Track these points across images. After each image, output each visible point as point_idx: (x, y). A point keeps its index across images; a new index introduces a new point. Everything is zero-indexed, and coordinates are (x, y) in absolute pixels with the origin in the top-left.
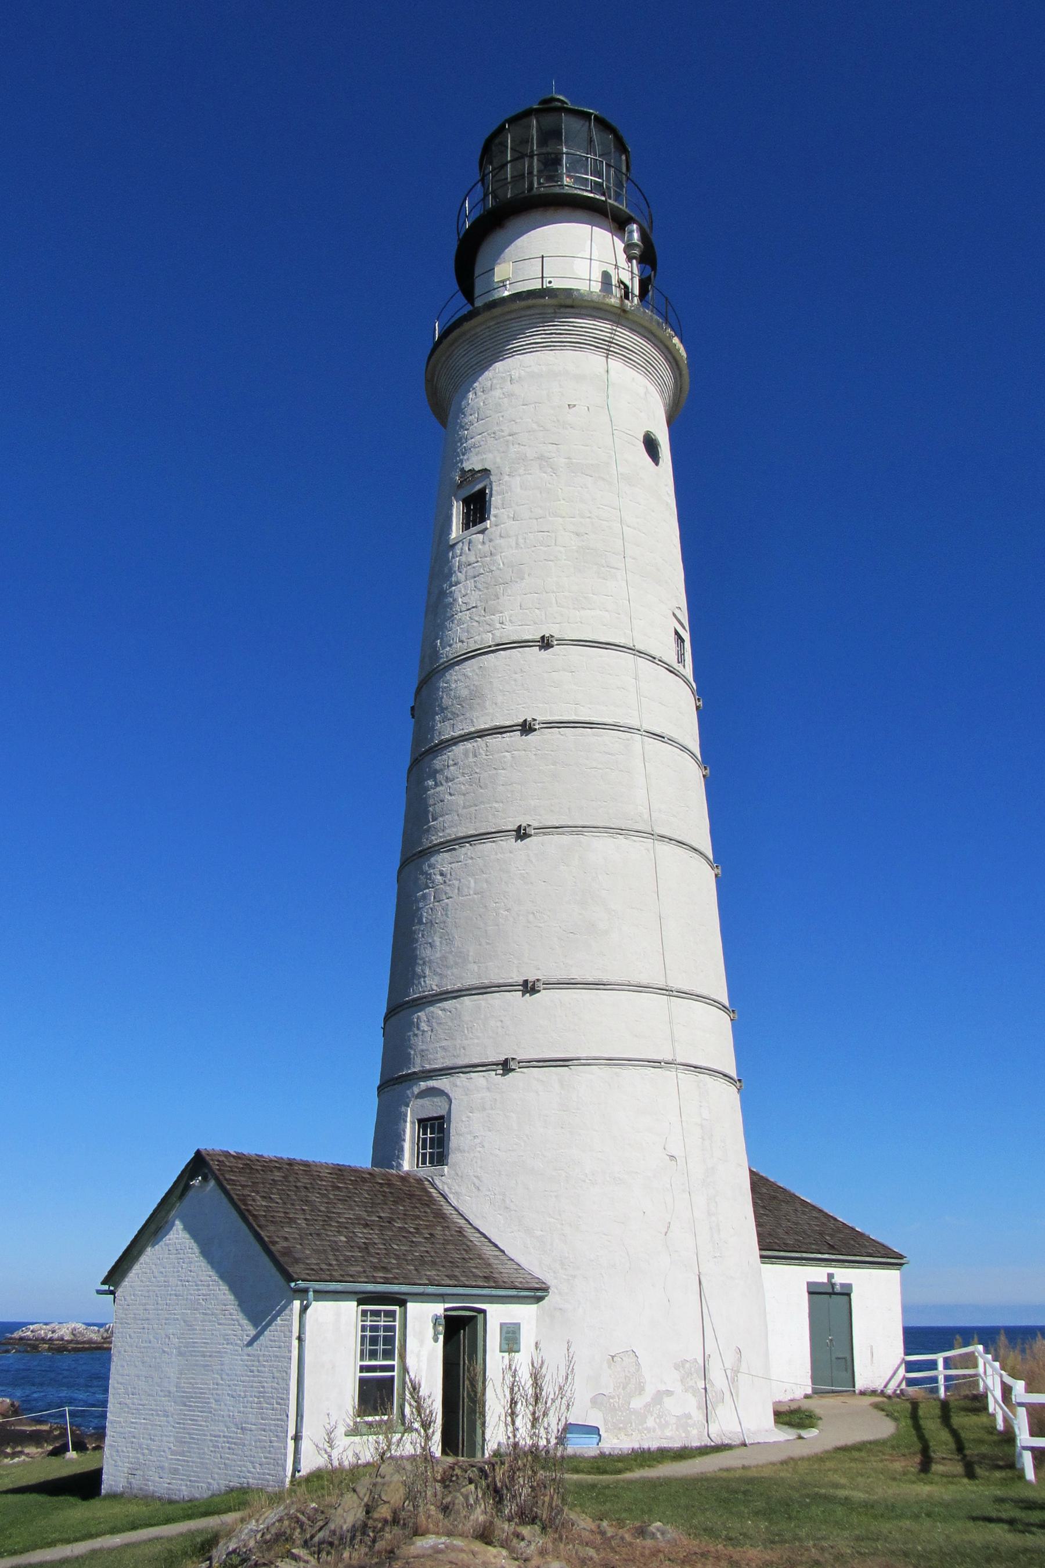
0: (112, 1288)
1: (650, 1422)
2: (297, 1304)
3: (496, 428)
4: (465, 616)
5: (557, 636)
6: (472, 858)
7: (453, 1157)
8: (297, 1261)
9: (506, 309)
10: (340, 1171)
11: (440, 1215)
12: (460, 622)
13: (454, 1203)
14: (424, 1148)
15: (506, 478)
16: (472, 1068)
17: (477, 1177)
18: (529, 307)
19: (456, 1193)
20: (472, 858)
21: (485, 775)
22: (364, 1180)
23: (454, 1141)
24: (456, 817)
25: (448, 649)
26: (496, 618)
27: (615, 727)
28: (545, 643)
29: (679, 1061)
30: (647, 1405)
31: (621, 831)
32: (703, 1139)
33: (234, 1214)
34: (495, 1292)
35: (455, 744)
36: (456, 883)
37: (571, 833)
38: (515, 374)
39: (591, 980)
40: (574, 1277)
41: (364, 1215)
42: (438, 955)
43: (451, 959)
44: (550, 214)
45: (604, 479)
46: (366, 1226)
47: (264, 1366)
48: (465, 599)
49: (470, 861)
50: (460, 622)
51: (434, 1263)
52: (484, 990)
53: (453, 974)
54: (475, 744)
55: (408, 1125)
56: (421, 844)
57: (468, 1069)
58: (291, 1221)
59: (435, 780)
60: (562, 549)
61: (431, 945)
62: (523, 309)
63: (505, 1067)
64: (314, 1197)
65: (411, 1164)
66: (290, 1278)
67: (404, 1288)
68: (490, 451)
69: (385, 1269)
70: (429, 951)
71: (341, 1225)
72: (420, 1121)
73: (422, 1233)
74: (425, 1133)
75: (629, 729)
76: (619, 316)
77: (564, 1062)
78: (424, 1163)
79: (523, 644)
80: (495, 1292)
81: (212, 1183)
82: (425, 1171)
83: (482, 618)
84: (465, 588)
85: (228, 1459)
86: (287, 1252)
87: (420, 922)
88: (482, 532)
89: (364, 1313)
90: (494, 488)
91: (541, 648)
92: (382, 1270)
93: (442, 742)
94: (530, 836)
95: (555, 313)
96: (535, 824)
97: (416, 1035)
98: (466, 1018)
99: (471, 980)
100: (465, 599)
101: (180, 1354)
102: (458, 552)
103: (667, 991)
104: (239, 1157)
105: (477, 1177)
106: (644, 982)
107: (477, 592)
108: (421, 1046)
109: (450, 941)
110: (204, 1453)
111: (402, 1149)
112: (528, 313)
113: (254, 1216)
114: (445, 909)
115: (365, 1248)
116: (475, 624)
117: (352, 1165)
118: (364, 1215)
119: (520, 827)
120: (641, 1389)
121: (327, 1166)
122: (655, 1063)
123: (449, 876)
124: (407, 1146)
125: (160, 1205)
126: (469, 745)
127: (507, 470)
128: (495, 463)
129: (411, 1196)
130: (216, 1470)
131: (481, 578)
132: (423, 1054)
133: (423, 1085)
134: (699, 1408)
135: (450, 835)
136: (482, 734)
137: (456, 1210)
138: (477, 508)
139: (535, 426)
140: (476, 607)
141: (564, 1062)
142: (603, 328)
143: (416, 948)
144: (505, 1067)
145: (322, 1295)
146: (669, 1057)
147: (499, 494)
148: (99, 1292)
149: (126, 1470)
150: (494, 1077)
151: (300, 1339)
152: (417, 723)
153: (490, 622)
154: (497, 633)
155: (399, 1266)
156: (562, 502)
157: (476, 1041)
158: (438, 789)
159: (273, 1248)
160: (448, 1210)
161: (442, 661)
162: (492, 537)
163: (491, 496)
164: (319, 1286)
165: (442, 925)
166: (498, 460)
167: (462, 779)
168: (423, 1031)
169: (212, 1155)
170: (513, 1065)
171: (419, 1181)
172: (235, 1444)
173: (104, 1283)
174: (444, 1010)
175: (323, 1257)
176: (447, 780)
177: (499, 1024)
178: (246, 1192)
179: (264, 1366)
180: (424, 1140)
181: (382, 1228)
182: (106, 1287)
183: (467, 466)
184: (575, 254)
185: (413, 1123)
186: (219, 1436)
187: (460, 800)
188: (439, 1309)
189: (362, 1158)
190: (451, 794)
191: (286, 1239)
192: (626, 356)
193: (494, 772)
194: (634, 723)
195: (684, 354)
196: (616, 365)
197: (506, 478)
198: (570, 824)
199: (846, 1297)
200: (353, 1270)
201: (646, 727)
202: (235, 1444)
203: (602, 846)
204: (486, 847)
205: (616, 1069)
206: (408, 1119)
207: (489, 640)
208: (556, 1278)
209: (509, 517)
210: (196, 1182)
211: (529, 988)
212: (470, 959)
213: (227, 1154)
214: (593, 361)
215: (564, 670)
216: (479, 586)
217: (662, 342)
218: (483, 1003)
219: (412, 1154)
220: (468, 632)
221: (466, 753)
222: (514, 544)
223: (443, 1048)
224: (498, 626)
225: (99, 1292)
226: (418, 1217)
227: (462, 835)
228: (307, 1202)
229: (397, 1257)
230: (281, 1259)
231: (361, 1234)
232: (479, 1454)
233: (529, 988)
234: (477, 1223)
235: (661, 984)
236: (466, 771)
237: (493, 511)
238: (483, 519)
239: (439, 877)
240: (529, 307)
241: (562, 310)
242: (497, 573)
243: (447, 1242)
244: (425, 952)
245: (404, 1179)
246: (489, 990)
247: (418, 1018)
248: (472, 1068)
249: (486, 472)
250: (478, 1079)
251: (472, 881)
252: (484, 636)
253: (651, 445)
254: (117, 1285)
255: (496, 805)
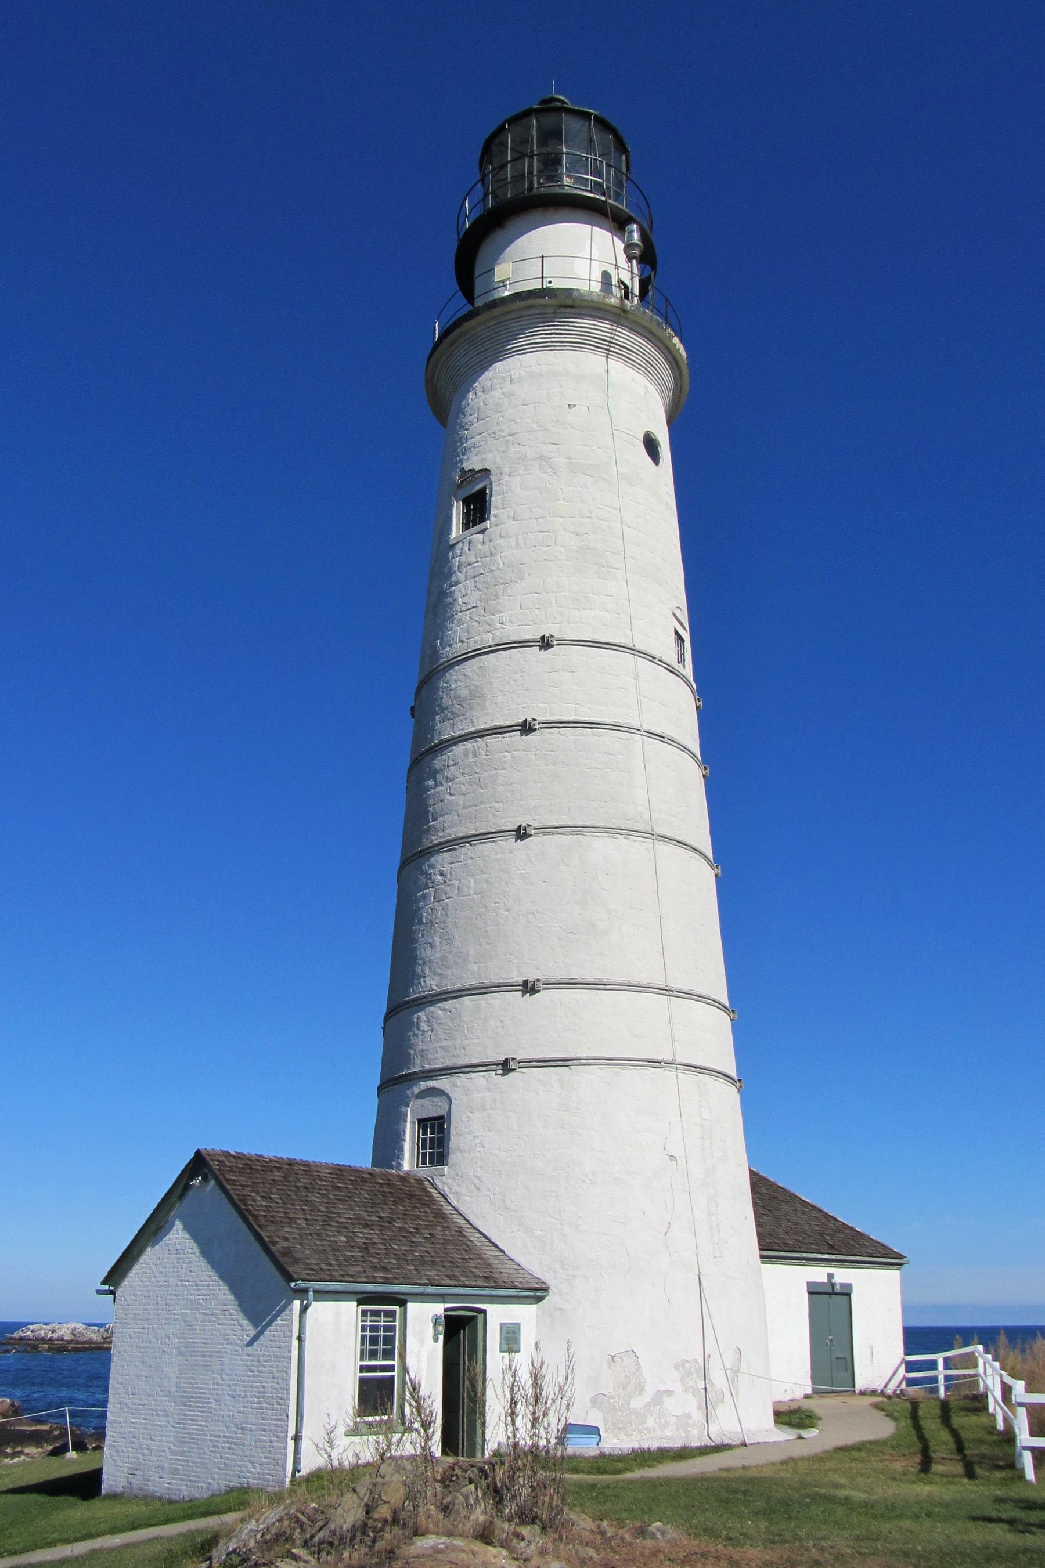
0: (112, 1288)
1: (650, 1422)
2: (297, 1304)
3: (496, 428)
4: (465, 616)
5: (557, 636)
6: (472, 858)
7: (453, 1157)
8: (297, 1261)
9: (506, 309)
10: (340, 1171)
11: (440, 1215)
12: (460, 622)
13: (454, 1203)
14: (424, 1148)
15: (506, 478)
16: (472, 1068)
17: (477, 1177)
18: (529, 307)
19: (456, 1193)
20: (472, 858)
21: (485, 775)
22: (364, 1180)
23: (454, 1141)
24: (456, 817)
25: (448, 649)
26: (496, 618)
27: (615, 727)
28: (545, 643)
29: (679, 1061)
30: (647, 1405)
31: (621, 831)
32: (703, 1139)
33: (234, 1214)
34: (495, 1292)
35: (455, 744)
36: (456, 883)
37: (571, 833)
38: (515, 374)
39: (591, 980)
40: (574, 1277)
41: (364, 1215)
42: (438, 955)
43: (451, 959)
44: (550, 214)
45: (604, 479)
46: (366, 1226)
47: (264, 1366)
48: (465, 599)
49: (470, 861)
50: (460, 622)
51: (434, 1263)
52: (484, 990)
53: (453, 974)
54: (475, 744)
55: (408, 1125)
56: (421, 844)
57: (468, 1069)
58: (291, 1221)
59: (435, 780)
60: (562, 549)
61: (431, 945)
62: (523, 309)
63: (505, 1067)
64: (314, 1197)
65: (411, 1164)
66: (290, 1278)
67: (404, 1288)
68: (490, 451)
69: (385, 1269)
70: (429, 951)
71: (341, 1225)
72: (420, 1121)
73: (422, 1233)
74: (425, 1133)
75: (629, 729)
76: (619, 316)
77: (564, 1062)
78: (424, 1163)
79: (523, 644)
80: (495, 1292)
81: (212, 1183)
82: (425, 1171)
83: (482, 618)
84: (465, 588)
85: (228, 1459)
86: (287, 1252)
87: (420, 922)
88: (482, 532)
89: (364, 1313)
90: (494, 488)
91: (541, 648)
92: (382, 1270)
93: (442, 742)
94: (530, 836)
95: (555, 313)
96: (535, 824)
97: (416, 1035)
98: (466, 1018)
99: (471, 980)
100: (465, 599)
101: (180, 1354)
102: (458, 552)
103: (667, 991)
104: (239, 1157)
105: (477, 1177)
106: (644, 982)
107: (477, 592)
108: (421, 1046)
109: (450, 941)
110: (204, 1453)
111: (402, 1149)
112: (528, 313)
113: (254, 1216)
114: (445, 909)
115: (365, 1248)
116: (475, 624)
117: (352, 1165)
118: (364, 1215)
119: (520, 827)
120: (641, 1389)
121: (327, 1166)
122: (655, 1063)
123: (449, 876)
124: (407, 1146)
125: (160, 1205)
126: (469, 745)
127: (507, 470)
128: (495, 463)
129: (411, 1196)
130: (216, 1470)
131: (481, 578)
132: (423, 1054)
133: (423, 1085)
134: (699, 1408)
135: (450, 835)
136: (482, 734)
137: (456, 1210)
138: (477, 508)
139: (535, 426)
140: (476, 607)
141: (564, 1062)
142: (603, 328)
143: (416, 948)
144: (505, 1067)
145: (322, 1295)
146: (669, 1057)
147: (499, 494)
148: (99, 1292)
149: (126, 1470)
150: (494, 1077)
151: (300, 1339)
152: (417, 723)
153: (490, 622)
154: (497, 633)
155: (399, 1266)
156: (562, 502)
157: (476, 1041)
158: (438, 789)
159: (273, 1248)
160: (448, 1210)
161: (442, 661)
162: (492, 537)
163: (491, 496)
164: (319, 1286)
165: (442, 925)
166: (498, 460)
167: (462, 779)
168: (423, 1031)
169: (212, 1155)
170: (513, 1065)
171: (419, 1181)
172: (235, 1444)
173: (104, 1283)
174: (444, 1010)
175: (323, 1257)
176: (447, 780)
177: (499, 1024)
178: (246, 1192)
179: (264, 1366)
180: (424, 1140)
181: (382, 1228)
182: (106, 1287)
183: (467, 466)
184: (575, 254)
185: (413, 1123)
186: (219, 1436)
187: (460, 800)
188: (439, 1309)
189: (362, 1158)
190: (451, 794)
191: (286, 1239)
192: (626, 356)
193: (494, 772)
194: (634, 723)
195: (684, 354)
196: (616, 365)
197: (506, 478)
198: (570, 824)
199: (846, 1297)
200: (353, 1270)
201: (646, 727)
202: (235, 1444)
203: (602, 846)
204: (486, 847)
205: (616, 1069)
206: (408, 1119)
207: (489, 640)
208: (556, 1278)
209: (509, 517)
210: (196, 1182)
211: (529, 988)
212: (470, 959)
213: (227, 1154)
214: (593, 361)
215: (564, 670)
216: (479, 586)
217: (662, 342)
218: (483, 1003)
219: (412, 1154)
220: (468, 632)
221: (466, 753)
222: (514, 544)
223: (443, 1048)
224: (498, 626)
225: (99, 1292)
226: (418, 1217)
227: (462, 835)
228: (307, 1202)
229: (397, 1257)
230: (281, 1259)
231: (361, 1234)
232: (479, 1454)
233: (529, 988)
234: (477, 1223)
235: (661, 984)
236: (466, 771)
237: (493, 511)
238: (483, 519)
239: (439, 877)
240: (529, 307)
241: (562, 310)
242: (497, 573)
243: (447, 1242)
244: (425, 952)
245: (404, 1179)
246: (489, 990)
247: (418, 1018)
248: (472, 1068)
249: (486, 472)
250: (478, 1079)
251: (472, 881)
252: (484, 636)
253: (651, 445)
254: (117, 1285)
255: (496, 805)
